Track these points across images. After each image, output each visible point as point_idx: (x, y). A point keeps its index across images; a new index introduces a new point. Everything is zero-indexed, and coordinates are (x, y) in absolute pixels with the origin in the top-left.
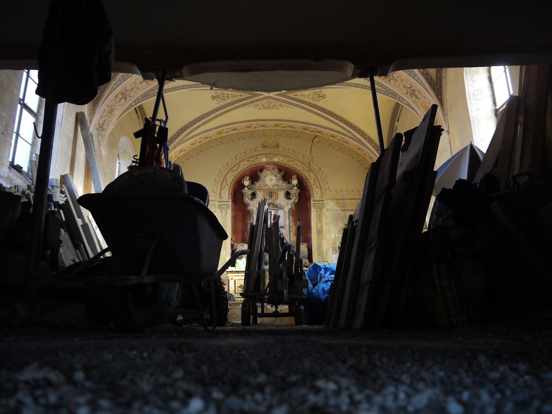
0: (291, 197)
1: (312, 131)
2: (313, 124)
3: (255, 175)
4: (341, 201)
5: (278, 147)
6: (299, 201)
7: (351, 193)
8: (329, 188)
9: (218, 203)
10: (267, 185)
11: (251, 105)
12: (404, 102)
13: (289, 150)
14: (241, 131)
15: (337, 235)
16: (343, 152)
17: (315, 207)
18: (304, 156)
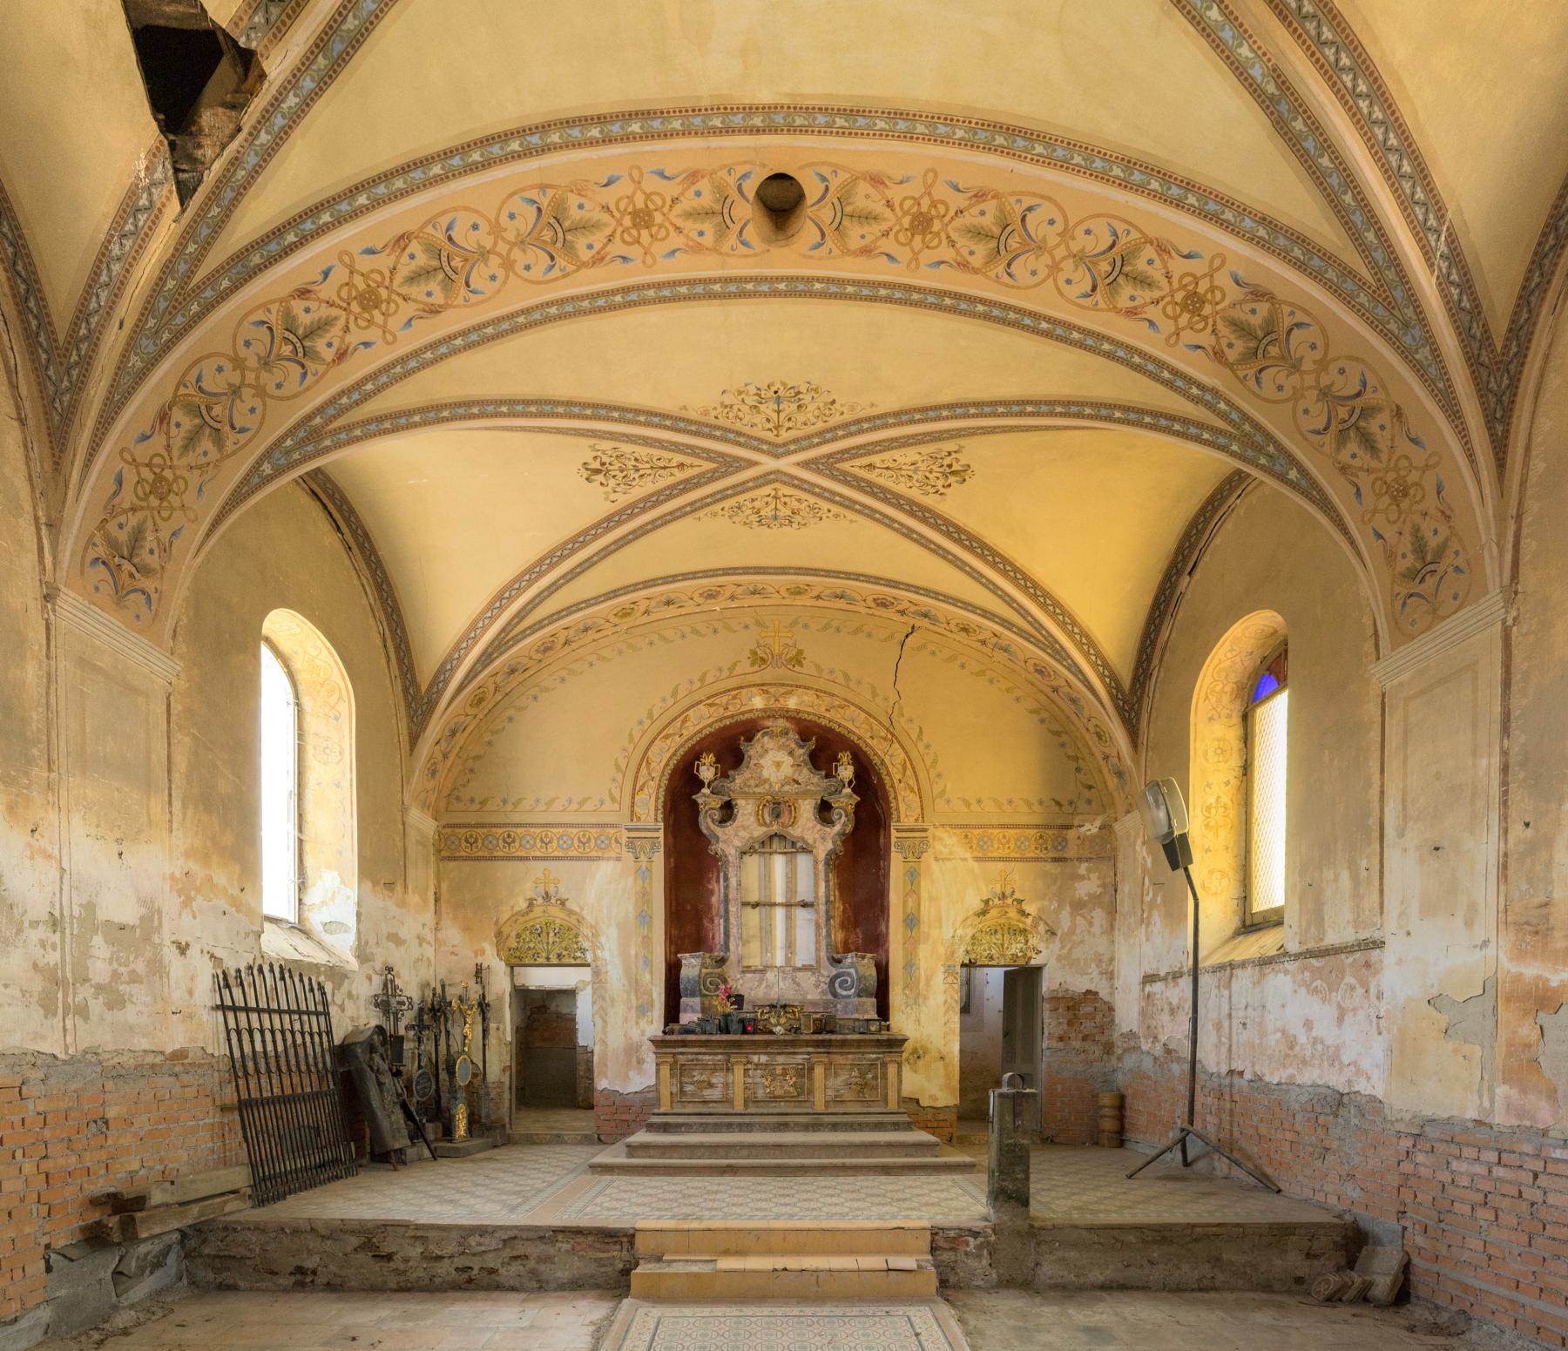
0: (835, 817)
1: (902, 613)
2: (909, 587)
3: (731, 746)
4: (976, 832)
5: (800, 664)
6: (855, 828)
7: (1006, 807)
8: (943, 792)
9: (625, 834)
10: (766, 781)
11: (717, 507)
12: (1293, 474)
13: (832, 672)
14: (690, 607)
15: (959, 932)
16: (991, 681)
17: (901, 848)
18: (874, 694)
